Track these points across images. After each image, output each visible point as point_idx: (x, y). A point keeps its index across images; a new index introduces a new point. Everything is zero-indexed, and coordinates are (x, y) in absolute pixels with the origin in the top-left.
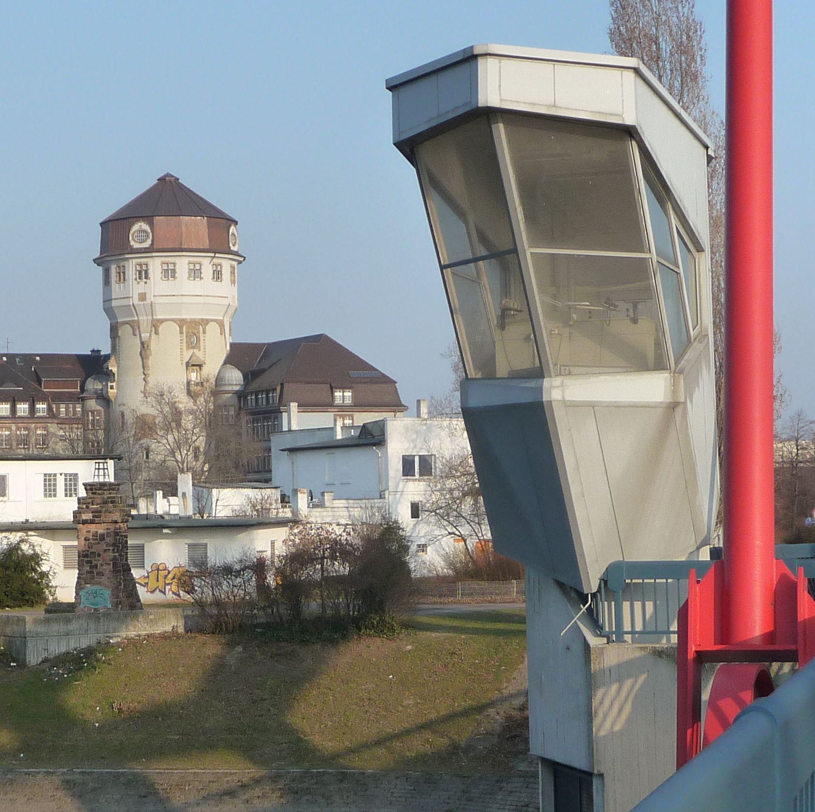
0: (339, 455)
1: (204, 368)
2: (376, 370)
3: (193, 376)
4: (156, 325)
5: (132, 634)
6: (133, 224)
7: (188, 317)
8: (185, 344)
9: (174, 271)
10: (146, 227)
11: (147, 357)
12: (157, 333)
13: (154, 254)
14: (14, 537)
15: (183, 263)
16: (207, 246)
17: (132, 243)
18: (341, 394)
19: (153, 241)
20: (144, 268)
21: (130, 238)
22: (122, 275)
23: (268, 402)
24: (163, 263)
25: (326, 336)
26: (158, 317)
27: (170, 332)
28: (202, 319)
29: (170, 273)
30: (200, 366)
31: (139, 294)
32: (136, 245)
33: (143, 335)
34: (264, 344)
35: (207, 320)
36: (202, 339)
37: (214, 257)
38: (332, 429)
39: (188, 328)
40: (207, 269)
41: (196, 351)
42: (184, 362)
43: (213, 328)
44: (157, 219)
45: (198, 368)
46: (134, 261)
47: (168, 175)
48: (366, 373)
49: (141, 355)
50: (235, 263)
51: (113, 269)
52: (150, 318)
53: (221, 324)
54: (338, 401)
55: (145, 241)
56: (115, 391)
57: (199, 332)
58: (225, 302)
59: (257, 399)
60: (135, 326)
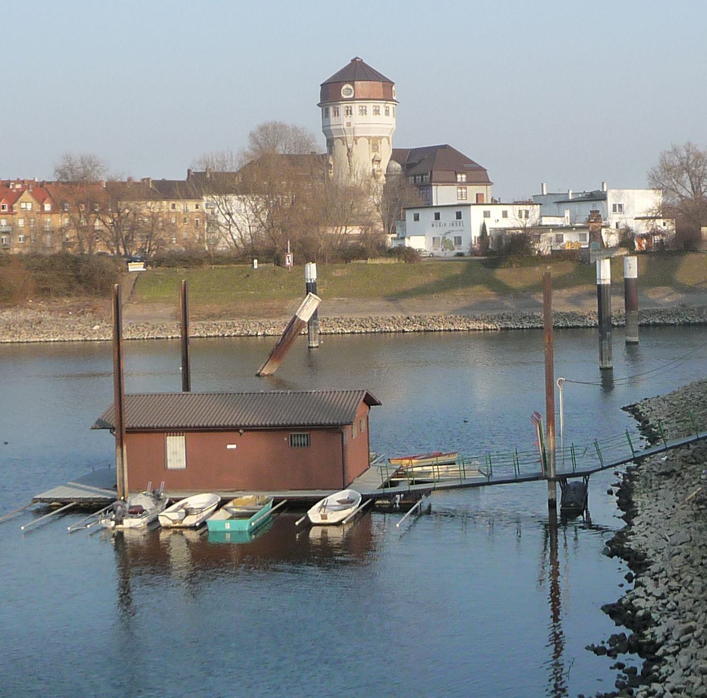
0: (570, 204)
1: (381, 162)
2: (476, 164)
3: (375, 167)
4: (356, 139)
5: (617, 255)
7: (373, 135)
10: (350, 87)
12: (356, 143)
15: (370, 106)
16: (382, 97)
17: (343, 95)
19: (354, 94)
20: (349, 109)
22: (336, 113)
23: (422, 181)
25: (449, 146)
26: (357, 135)
27: (363, 142)
28: (380, 136)
29: (364, 112)
30: (379, 161)
31: (347, 123)
32: (345, 97)
34: (408, 149)
38: (568, 194)
40: (382, 110)
41: (377, 153)
43: (384, 141)
44: (356, 83)
46: (344, 105)
47: (357, 58)
48: (470, 165)
49: (348, 155)
50: (394, 106)
51: (331, 109)
52: (352, 135)
53: (388, 138)
54: (459, 180)
55: (350, 94)
56: (332, 174)
58: (391, 127)
59: (422, 178)
60: (344, 140)
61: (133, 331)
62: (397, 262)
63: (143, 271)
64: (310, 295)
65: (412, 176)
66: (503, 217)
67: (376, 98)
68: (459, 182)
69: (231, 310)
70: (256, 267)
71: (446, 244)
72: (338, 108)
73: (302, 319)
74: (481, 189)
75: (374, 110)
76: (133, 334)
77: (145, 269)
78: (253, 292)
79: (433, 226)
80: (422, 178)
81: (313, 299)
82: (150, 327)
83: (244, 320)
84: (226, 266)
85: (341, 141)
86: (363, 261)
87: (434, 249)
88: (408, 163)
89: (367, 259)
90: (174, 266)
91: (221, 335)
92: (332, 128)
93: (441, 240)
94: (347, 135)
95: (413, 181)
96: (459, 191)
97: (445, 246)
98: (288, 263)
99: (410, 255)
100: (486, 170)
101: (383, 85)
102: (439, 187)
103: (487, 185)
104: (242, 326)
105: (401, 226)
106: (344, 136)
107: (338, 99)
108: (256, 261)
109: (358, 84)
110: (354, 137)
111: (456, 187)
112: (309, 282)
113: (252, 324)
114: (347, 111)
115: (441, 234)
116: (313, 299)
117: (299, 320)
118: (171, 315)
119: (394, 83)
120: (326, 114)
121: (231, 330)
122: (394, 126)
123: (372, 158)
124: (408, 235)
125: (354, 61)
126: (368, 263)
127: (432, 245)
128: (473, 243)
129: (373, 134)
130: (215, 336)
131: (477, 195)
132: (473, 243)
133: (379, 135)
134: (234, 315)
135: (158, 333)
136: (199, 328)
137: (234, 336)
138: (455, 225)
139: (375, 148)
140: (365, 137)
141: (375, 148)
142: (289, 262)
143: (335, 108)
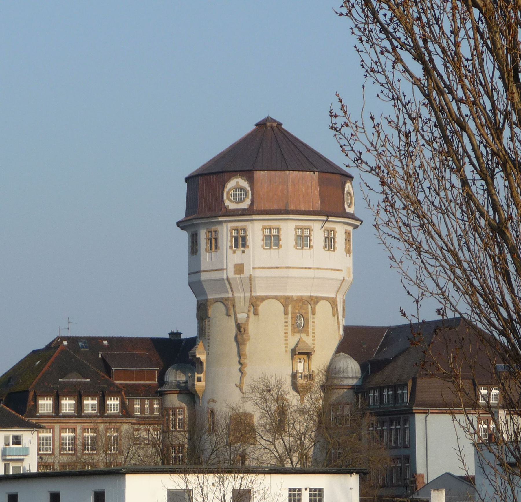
3: (300, 367)
4: (255, 303)
6: (228, 180)
8: (290, 328)
9: (278, 238)
10: (243, 183)
11: (244, 344)
12: (256, 313)
15: (288, 228)
16: (317, 206)
17: (227, 203)
22: (214, 243)
24: (264, 228)
28: (311, 297)
29: (273, 240)
30: (308, 354)
31: (235, 266)
32: (231, 206)
33: (239, 316)
35: (317, 298)
36: (310, 321)
37: (327, 221)
39: (294, 307)
40: (318, 236)
41: (303, 336)
43: (323, 308)
44: (259, 175)
45: (305, 357)
46: (230, 225)
47: (268, 119)
50: (350, 228)
51: (203, 234)
52: (248, 294)
53: (333, 302)
57: (307, 313)
59: (395, 395)
60: (229, 305)
72: (216, 232)
80: (395, 395)
94: (236, 295)
101: (321, 182)
102: (431, 418)
106: (230, 295)
110: (252, 297)
114: (236, 239)
123: (292, 345)
140: (276, 298)
143: (210, 232)
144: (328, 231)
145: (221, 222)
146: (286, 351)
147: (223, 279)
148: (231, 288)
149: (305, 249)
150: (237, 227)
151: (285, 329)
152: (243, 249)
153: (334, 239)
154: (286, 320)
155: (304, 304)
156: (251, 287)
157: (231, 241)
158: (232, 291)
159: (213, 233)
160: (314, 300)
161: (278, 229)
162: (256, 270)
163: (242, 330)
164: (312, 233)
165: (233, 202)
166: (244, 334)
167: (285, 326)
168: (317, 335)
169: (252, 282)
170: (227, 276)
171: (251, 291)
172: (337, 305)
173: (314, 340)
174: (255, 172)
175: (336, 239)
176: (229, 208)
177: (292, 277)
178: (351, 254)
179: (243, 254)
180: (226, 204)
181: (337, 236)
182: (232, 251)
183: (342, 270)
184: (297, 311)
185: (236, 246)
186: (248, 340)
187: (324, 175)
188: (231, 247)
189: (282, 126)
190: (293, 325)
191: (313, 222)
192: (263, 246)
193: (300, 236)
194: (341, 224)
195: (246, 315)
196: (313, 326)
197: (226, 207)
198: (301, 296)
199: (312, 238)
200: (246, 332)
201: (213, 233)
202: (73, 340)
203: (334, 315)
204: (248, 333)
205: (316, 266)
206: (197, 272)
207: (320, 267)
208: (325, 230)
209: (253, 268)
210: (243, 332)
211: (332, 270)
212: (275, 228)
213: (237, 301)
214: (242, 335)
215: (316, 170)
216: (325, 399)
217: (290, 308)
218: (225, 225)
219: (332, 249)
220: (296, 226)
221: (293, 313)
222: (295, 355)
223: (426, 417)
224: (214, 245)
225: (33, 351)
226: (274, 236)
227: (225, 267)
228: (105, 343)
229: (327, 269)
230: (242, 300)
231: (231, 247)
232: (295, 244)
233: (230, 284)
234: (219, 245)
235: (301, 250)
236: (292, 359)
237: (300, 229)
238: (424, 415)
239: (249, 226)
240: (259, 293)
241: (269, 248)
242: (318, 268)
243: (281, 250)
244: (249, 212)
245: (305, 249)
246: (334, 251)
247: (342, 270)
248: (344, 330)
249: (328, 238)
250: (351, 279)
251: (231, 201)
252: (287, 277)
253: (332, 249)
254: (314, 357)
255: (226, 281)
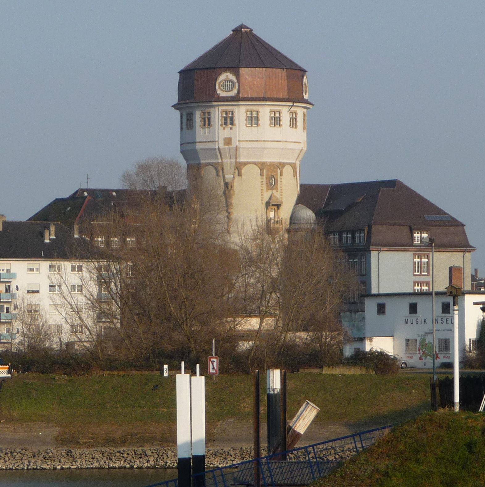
3: (272, 214)
4: (239, 167)
6: (220, 74)
8: (265, 186)
9: (257, 119)
10: (232, 77)
11: (231, 197)
12: (240, 175)
13: (241, 103)
14: (445, 376)
15: (265, 111)
16: (286, 96)
17: (219, 91)
18: (419, 235)
19: (239, 90)
21: (217, 87)
22: (207, 121)
24: (247, 111)
27: (252, 174)
28: (280, 163)
29: (253, 120)
30: (278, 206)
31: (225, 139)
32: (222, 94)
33: (226, 176)
35: (283, 163)
36: (279, 180)
37: (293, 106)
39: (268, 170)
40: (286, 118)
41: (274, 192)
42: (264, 202)
43: (288, 170)
44: (242, 71)
45: (276, 207)
46: (221, 108)
47: (242, 26)
48: (434, 217)
50: (305, 110)
51: (198, 115)
52: (233, 160)
53: (293, 166)
54: (417, 242)
55: (231, 90)
57: (277, 175)
59: (353, 238)
60: (219, 168)
61: (7, 459)
62: (364, 372)
63: (8, 378)
64: (308, 403)
65: (334, 233)
66: (474, 303)
67: (275, 96)
68: (417, 246)
69: (137, 434)
70: (166, 375)
71: (425, 349)
72: (209, 113)
73: (298, 431)
74: (454, 258)
75: (272, 118)
76: (7, 463)
77: (9, 375)
78: (165, 410)
79: (406, 322)
80: (353, 238)
81: (310, 407)
82: (30, 454)
83: (158, 447)
84: (122, 373)
85: (213, 171)
86: (316, 371)
87: (408, 357)
88: (328, 209)
89: (322, 367)
90: (50, 371)
91: (128, 466)
92: (198, 146)
93: (418, 343)
94: (224, 160)
95: (337, 242)
96: (417, 260)
97: (424, 353)
98: (211, 371)
99: (380, 361)
100: (463, 225)
101: (288, 77)
102: (382, 254)
103: (464, 252)
104: (157, 456)
105: (350, 322)
106: (220, 161)
107: (210, 97)
108: (166, 366)
109: (244, 72)
110: (236, 163)
111: (410, 254)
112: (272, 392)
113: (170, 452)
114: (226, 119)
115: (418, 335)
116: (310, 407)
117: (295, 431)
118: (56, 438)
119: (305, 71)
120: (187, 123)
121: (141, 460)
122: (303, 146)
123: (266, 199)
124: (367, 334)
125: (237, 31)
126: (324, 373)
127: (404, 349)
128: (467, 348)
129: (269, 156)
130: (120, 468)
131: (451, 269)
132: (467, 348)
133: (278, 161)
134: (142, 440)
135: (42, 461)
136: (97, 456)
137: (147, 468)
138: (440, 321)
139: (272, 182)
140: (255, 163)
141: (272, 182)
142: (213, 368)
143: (204, 113)
144: (292, 113)
145: (214, 106)
146: (262, 203)
147: (215, 149)
148: (221, 155)
149: (277, 127)
150: (226, 109)
151: (261, 187)
152: (230, 126)
153: (296, 119)
154: (262, 180)
155: (274, 168)
156: (236, 155)
157: (221, 120)
158: (221, 158)
159: (207, 114)
160: (281, 165)
161: (257, 112)
162: (242, 142)
163: (229, 187)
164: (282, 115)
165: (223, 91)
166: (231, 190)
167: (262, 184)
168: (283, 191)
169: (238, 151)
170: (219, 147)
171: (236, 158)
172: (296, 168)
173: (281, 195)
174: (240, 68)
175: (298, 119)
176: (221, 95)
177: (267, 148)
178: (306, 130)
179: (231, 130)
180: (218, 92)
181: (298, 117)
182: (222, 128)
183: (301, 143)
184: (270, 173)
185: (226, 124)
186: (234, 194)
187: (290, 71)
188: (221, 125)
189: (253, 32)
190: (267, 183)
191: (282, 107)
192: (246, 125)
193: (273, 117)
194: (301, 108)
195: (232, 176)
196: (281, 184)
197: (218, 95)
198: (273, 162)
199: (281, 118)
200: (232, 189)
201: (207, 114)
202: (92, 192)
203: (294, 176)
204: (233, 190)
205: (284, 140)
206: (192, 143)
207: (287, 140)
208: (291, 112)
209: (239, 141)
210: (230, 188)
211: (295, 142)
212: (255, 111)
213: (225, 165)
214: (229, 191)
215: (284, 67)
216: (289, 239)
217: (265, 170)
218: (217, 108)
219: (295, 127)
220: (270, 110)
221: (267, 175)
222: (269, 206)
223: (379, 253)
224: (207, 123)
225: (56, 199)
226: (254, 117)
227: (217, 140)
228: (114, 194)
229: (291, 142)
230: (229, 164)
231: (221, 125)
232: (269, 123)
233: (220, 153)
234: (212, 123)
235: (274, 128)
236: (267, 209)
237: (273, 112)
238: (377, 252)
239: (236, 109)
240: (242, 159)
241: (250, 126)
242: (286, 142)
243: (259, 127)
244: (236, 99)
245: (277, 127)
246: (296, 128)
247: (301, 143)
248: (300, 187)
249: (292, 118)
250: (306, 149)
251: (222, 90)
252: (264, 148)
253: (295, 127)
254: (282, 208)
255: (217, 150)
